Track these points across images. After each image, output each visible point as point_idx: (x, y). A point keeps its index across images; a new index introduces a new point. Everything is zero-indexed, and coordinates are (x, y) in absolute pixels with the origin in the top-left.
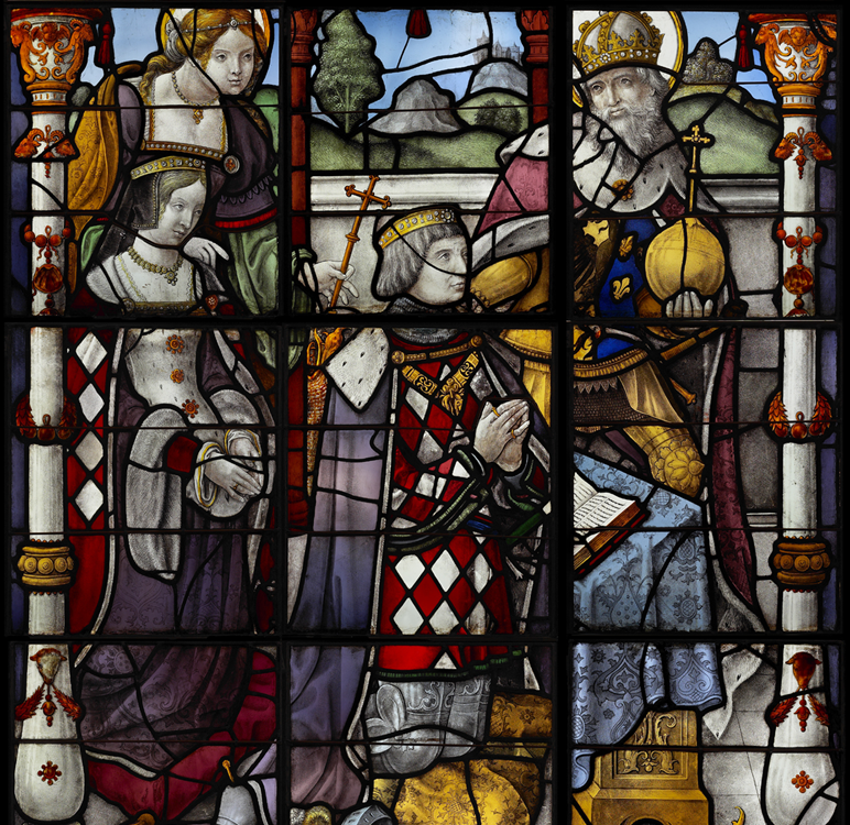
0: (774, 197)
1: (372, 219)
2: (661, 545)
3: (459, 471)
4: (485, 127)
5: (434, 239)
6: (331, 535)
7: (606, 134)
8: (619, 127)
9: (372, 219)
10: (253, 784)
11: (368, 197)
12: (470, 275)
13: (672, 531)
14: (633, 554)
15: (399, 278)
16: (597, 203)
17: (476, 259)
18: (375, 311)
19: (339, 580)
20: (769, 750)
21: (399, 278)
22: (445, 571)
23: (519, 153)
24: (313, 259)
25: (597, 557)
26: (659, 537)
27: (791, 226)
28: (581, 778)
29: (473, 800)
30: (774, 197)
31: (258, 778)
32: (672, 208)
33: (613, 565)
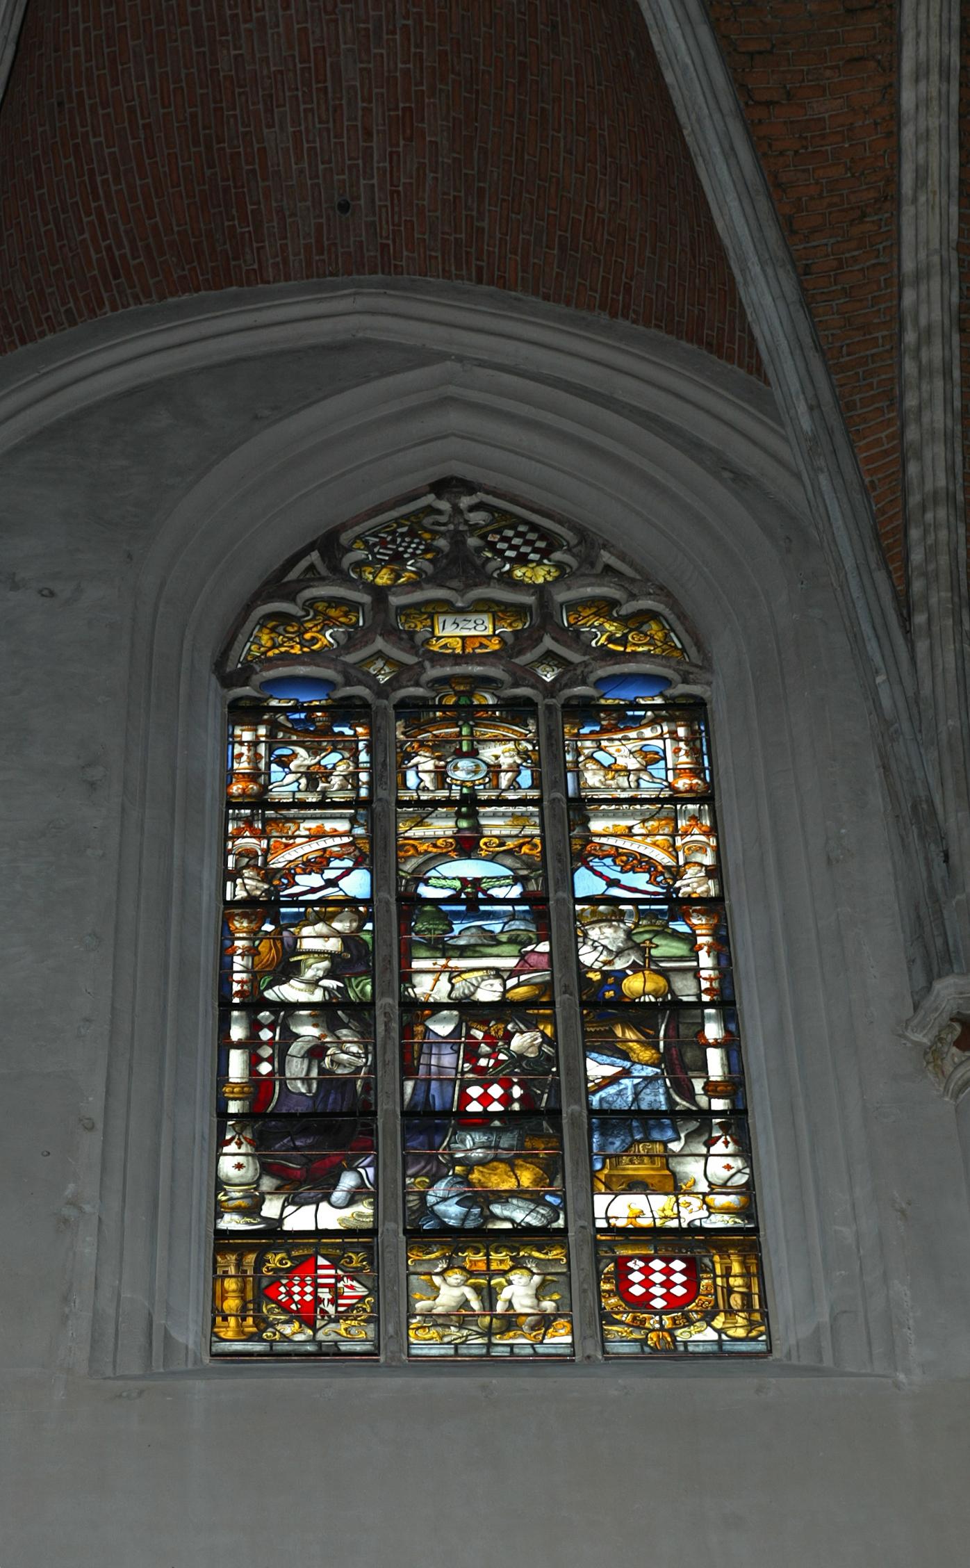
0: (695, 964)
1: (447, 974)
2: (639, 1083)
3: (502, 1057)
5: (483, 980)
7: (596, 944)
8: (605, 942)
9: (447, 974)
10: (360, 1170)
11: (446, 966)
12: (505, 991)
14: (622, 1087)
15: (464, 993)
17: (508, 987)
19: (433, 1096)
20: (706, 1157)
21: (464, 993)
23: (533, 951)
24: (414, 987)
27: (704, 974)
28: (598, 1166)
29: (515, 1175)
30: (695, 964)
31: (363, 1167)
32: (635, 967)
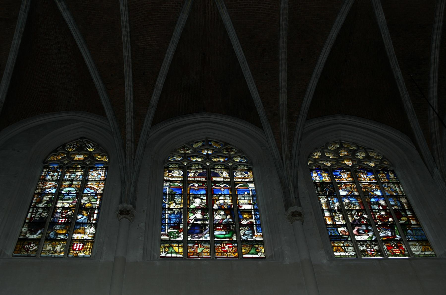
4: (72, 199)
6: (55, 218)
13: (85, 218)
16: (233, 240)
18: (249, 183)
20: (90, 229)
22: (25, 247)
25: (78, 219)
26: (83, 218)
33: (80, 220)
